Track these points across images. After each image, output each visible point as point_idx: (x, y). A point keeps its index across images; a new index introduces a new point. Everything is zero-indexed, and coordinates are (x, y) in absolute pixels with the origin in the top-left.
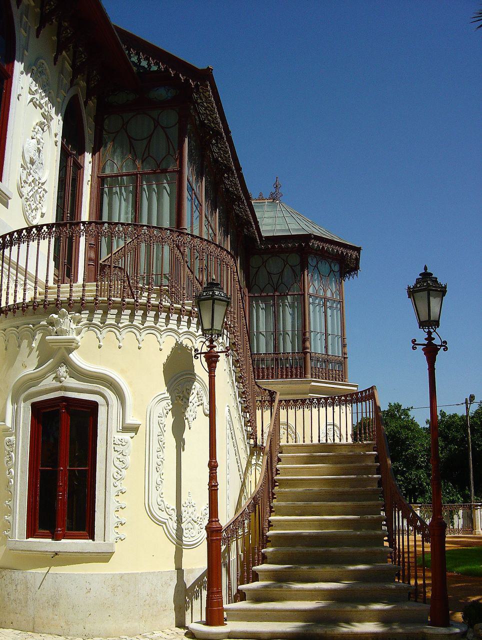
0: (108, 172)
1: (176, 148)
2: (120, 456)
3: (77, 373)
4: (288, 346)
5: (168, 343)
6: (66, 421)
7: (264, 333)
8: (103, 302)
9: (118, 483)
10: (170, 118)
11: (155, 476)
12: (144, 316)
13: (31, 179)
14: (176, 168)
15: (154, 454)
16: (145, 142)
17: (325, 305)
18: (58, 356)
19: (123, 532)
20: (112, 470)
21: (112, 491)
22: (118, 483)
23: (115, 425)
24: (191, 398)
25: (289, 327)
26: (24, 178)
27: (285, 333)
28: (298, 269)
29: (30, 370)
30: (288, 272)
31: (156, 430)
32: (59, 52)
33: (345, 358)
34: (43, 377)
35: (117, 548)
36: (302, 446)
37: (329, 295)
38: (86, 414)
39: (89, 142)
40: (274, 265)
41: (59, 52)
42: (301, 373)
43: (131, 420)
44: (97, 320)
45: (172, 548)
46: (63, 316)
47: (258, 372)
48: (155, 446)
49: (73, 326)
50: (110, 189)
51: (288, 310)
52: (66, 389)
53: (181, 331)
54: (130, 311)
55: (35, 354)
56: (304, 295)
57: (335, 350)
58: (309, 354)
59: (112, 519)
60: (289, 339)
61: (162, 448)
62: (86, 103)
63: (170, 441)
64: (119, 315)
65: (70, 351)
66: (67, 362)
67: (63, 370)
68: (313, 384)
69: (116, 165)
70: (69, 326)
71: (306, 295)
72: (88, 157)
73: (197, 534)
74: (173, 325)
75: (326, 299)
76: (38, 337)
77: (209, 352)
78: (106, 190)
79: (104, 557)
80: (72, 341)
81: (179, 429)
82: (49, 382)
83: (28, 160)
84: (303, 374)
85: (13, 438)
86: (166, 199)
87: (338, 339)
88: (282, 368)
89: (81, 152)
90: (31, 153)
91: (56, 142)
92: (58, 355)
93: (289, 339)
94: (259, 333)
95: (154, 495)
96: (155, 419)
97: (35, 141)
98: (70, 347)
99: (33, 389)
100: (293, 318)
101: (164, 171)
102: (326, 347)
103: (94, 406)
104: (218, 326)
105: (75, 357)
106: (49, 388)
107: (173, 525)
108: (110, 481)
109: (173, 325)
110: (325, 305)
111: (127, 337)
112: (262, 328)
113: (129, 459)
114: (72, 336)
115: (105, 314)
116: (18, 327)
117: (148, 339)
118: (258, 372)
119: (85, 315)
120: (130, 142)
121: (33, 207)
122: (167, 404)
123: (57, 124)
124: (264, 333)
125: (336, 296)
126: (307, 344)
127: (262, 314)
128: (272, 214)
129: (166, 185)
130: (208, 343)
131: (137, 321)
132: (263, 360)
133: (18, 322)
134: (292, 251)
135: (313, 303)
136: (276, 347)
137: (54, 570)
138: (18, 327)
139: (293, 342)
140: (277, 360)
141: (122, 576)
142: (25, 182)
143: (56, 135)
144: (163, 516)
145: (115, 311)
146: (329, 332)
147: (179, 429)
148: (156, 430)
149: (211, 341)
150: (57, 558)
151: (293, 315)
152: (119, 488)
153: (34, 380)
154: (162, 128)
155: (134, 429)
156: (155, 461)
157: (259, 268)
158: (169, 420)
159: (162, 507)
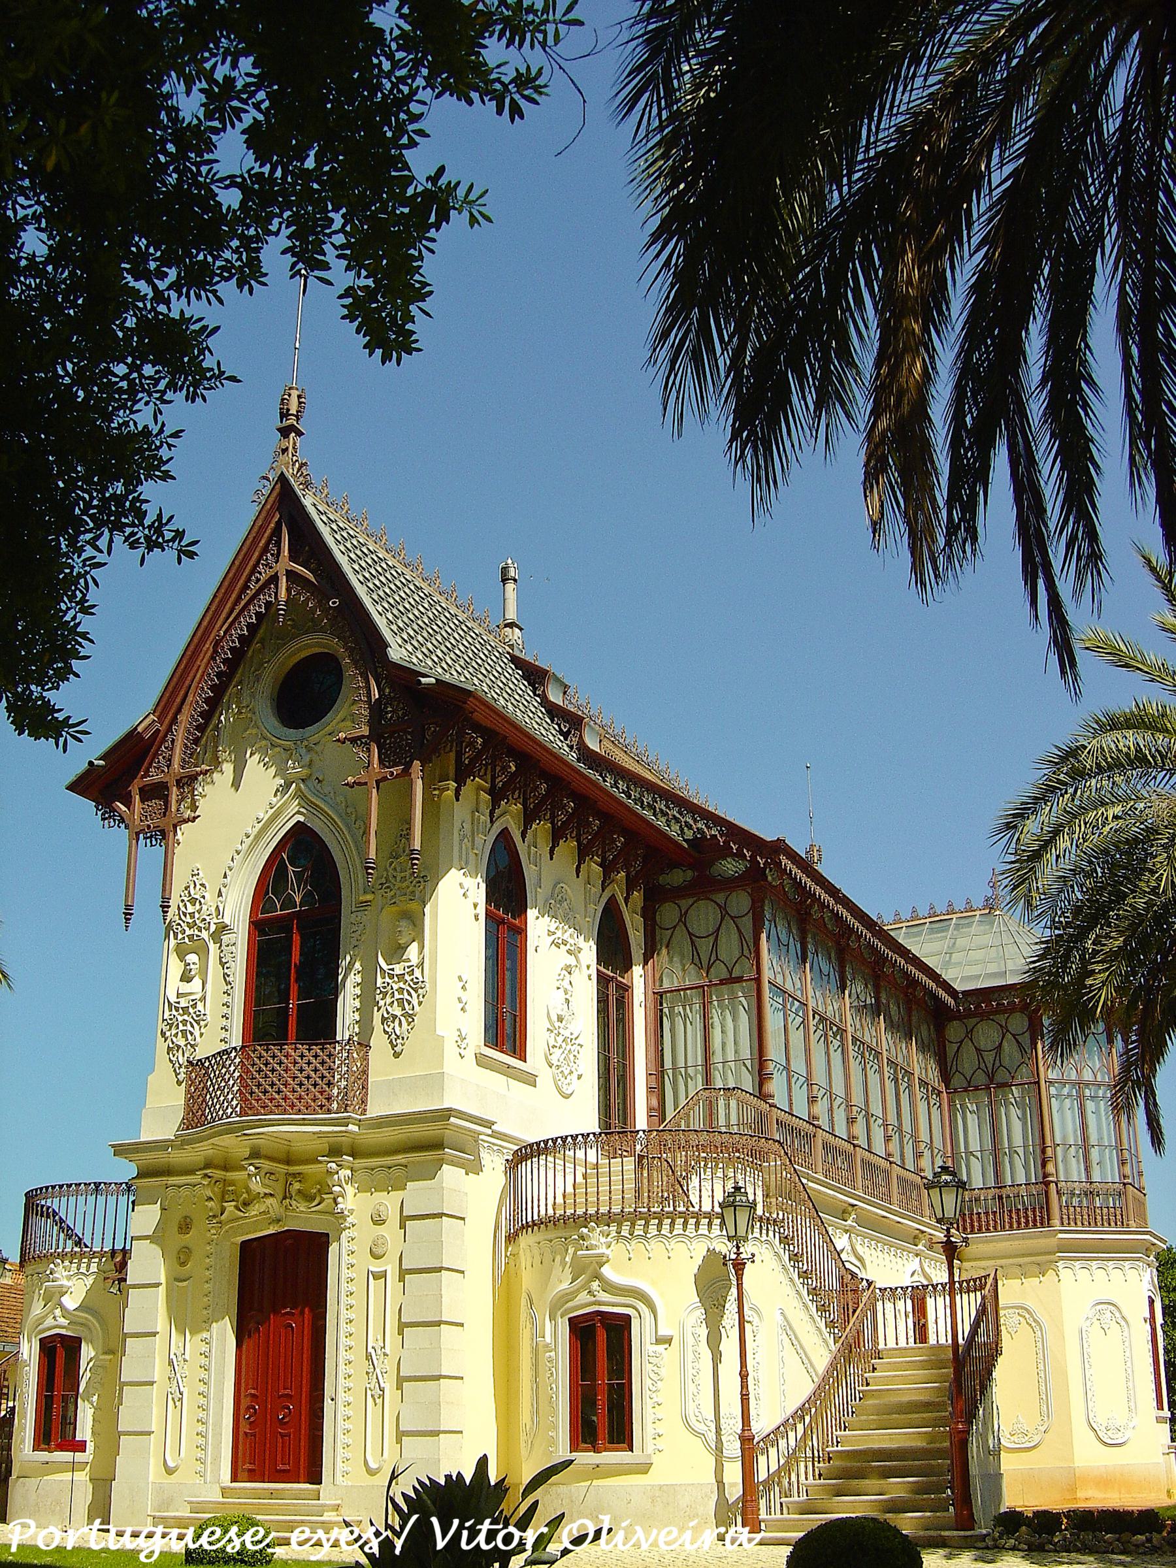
0: (666, 985)
1: (751, 944)
2: (655, 1368)
3: (608, 1287)
4: (1019, 1173)
5: (700, 1250)
6: (602, 1336)
7: (979, 1154)
8: (630, 1213)
9: (654, 1395)
10: (740, 902)
11: (691, 1388)
12: (673, 1224)
13: (560, 1039)
14: (753, 975)
15: (689, 1365)
16: (712, 939)
17: (1081, 1099)
18: (589, 1272)
19: (660, 1443)
20: (648, 1382)
21: (649, 1403)
22: (654, 1395)
23: (648, 1337)
24: (727, 1306)
25: (1018, 1140)
26: (552, 1043)
27: (1013, 1151)
28: (1026, 1039)
29: (565, 1285)
30: (1009, 1047)
31: (690, 1340)
32: (581, 861)
33: (1125, 1184)
34: (578, 1291)
35: (656, 1459)
36: (905, 1349)
37: (1087, 1076)
38: (616, 1330)
39: (637, 952)
40: (987, 1035)
41: (581, 861)
42: (1042, 1218)
43: (662, 1332)
44: (625, 1232)
45: (711, 1461)
46: (592, 1230)
47: (972, 1220)
48: (690, 1357)
49: (603, 1240)
50: (671, 1009)
51: (1014, 1112)
52: (600, 1303)
53: (712, 1236)
54: (643, 1222)
55: (568, 1270)
56: (1038, 1083)
57: (1106, 1172)
58: (1053, 1186)
59: (650, 1430)
60: (1019, 1163)
61: (697, 1358)
62: (626, 900)
63: (706, 1354)
64: (647, 1225)
65: (601, 1265)
66: (598, 1276)
67: (595, 1285)
68: (1060, 1236)
69: (676, 973)
70: (599, 1240)
71: (1042, 1083)
72: (637, 970)
73: (733, 1447)
74: (703, 1229)
75: (1080, 1084)
76: (571, 1250)
77: (736, 1259)
78: (666, 1010)
79: (644, 1468)
80: (602, 1255)
81: (714, 1341)
82: (583, 1297)
83: (554, 1018)
84: (1046, 1221)
85: (553, 1354)
86: (744, 1018)
87: (1111, 1152)
88: (1010, 1211)
89: (627, 967)
90: (558, 1008)
91: (590, 976)
92: (589, 1270)
93: (1019, 1163)
94: (970, 1154)
95: (691, 1407)
96: (689, 1331)
97: (562, 990)
98: (601, 1261)
99: (570, 1304)
100: (1024, 1124)
101: (739, 980)
102: (1088, 1169)
103: (629, 1317)
104: (741, 1231)
105: (606, 1271)
106: (583, 1304)
107: (712, 1436)
108: (647, 1393)
109: (703, 1229)
110: (1081, 1099)
111: (656, 1246)
112: (974, 1146)
113: (663, 1372)
114: (603, 1250)
115: (633, 1225)
116: (551, 1241)
117: (678, 1248)
118: (972, 1220)
119: (613, 1228)
120: (692, 942)
121: (566, 1072)
122: (700, 1313)
123: (589, 951)
124: (979, 1154)
125: (1103, 1077)
126: (1050, 1168)
127: (972, 1120)
128: (988, 939)
129: (742, 999)
130: (735, 1250)
131: (665, 1229)
132: (977, 1200)
133: (551, 1235)
134: (1012, 1009)
135: (1057, 1096)
136: (997, 1174)
137: (595, 1482)
138: (551, 1241)
139: (1026, 1167)
140: (1000, 1198)
141: (661, 1487)
142: (554, 1047)
143: (588, 967)
144: (700, 1427)
145: (643, 1222)
146: (1093, 1139)
147: (714, 1341)
148: (690, 1340)
149: (738, 1248)
150: (598, 1471)
151: (1023, 1119)
152: (655, 1399)
153: (573, 1295)
154: (732, 918)
155: (668, 1341)
156: (690, 1372)
157: (961, 1042)
158: (703, 1331)
159: (700, 1419)
